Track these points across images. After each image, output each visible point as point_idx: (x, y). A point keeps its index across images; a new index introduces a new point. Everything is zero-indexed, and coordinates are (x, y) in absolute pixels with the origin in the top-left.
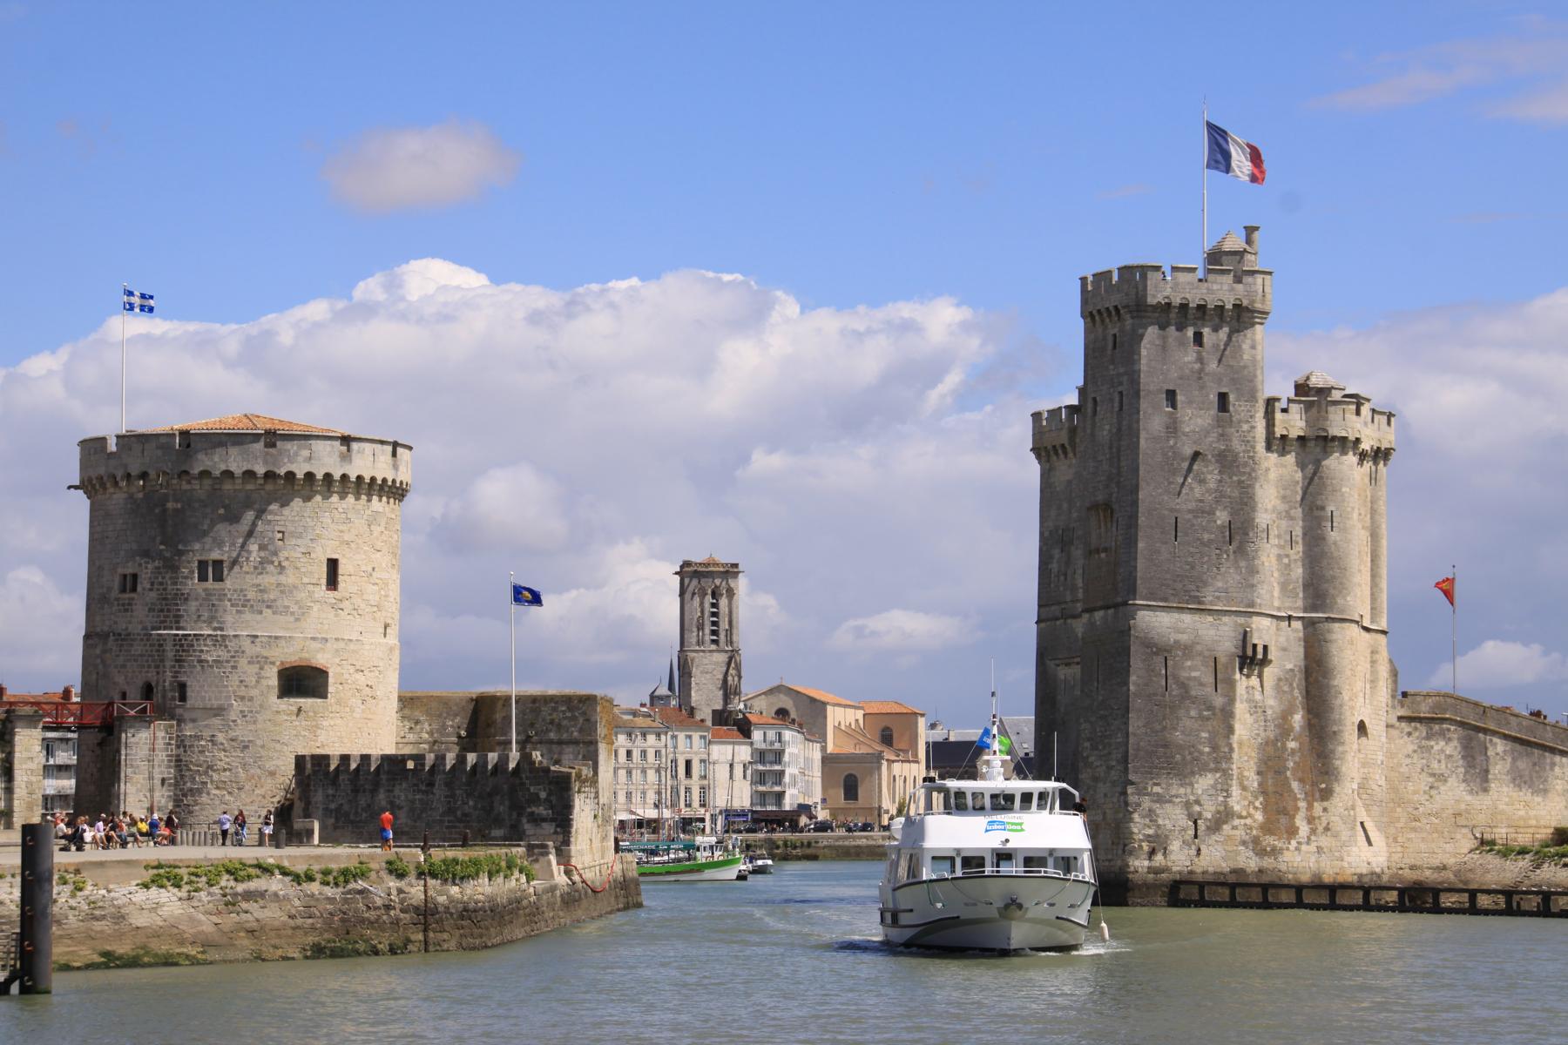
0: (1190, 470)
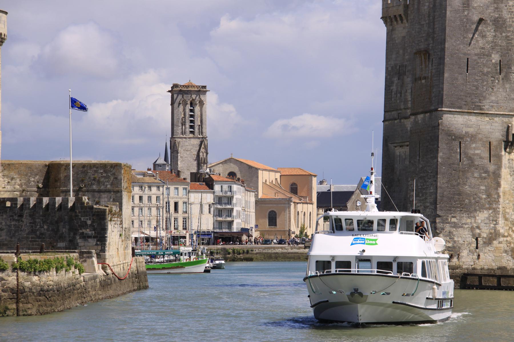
0: (476, 29)
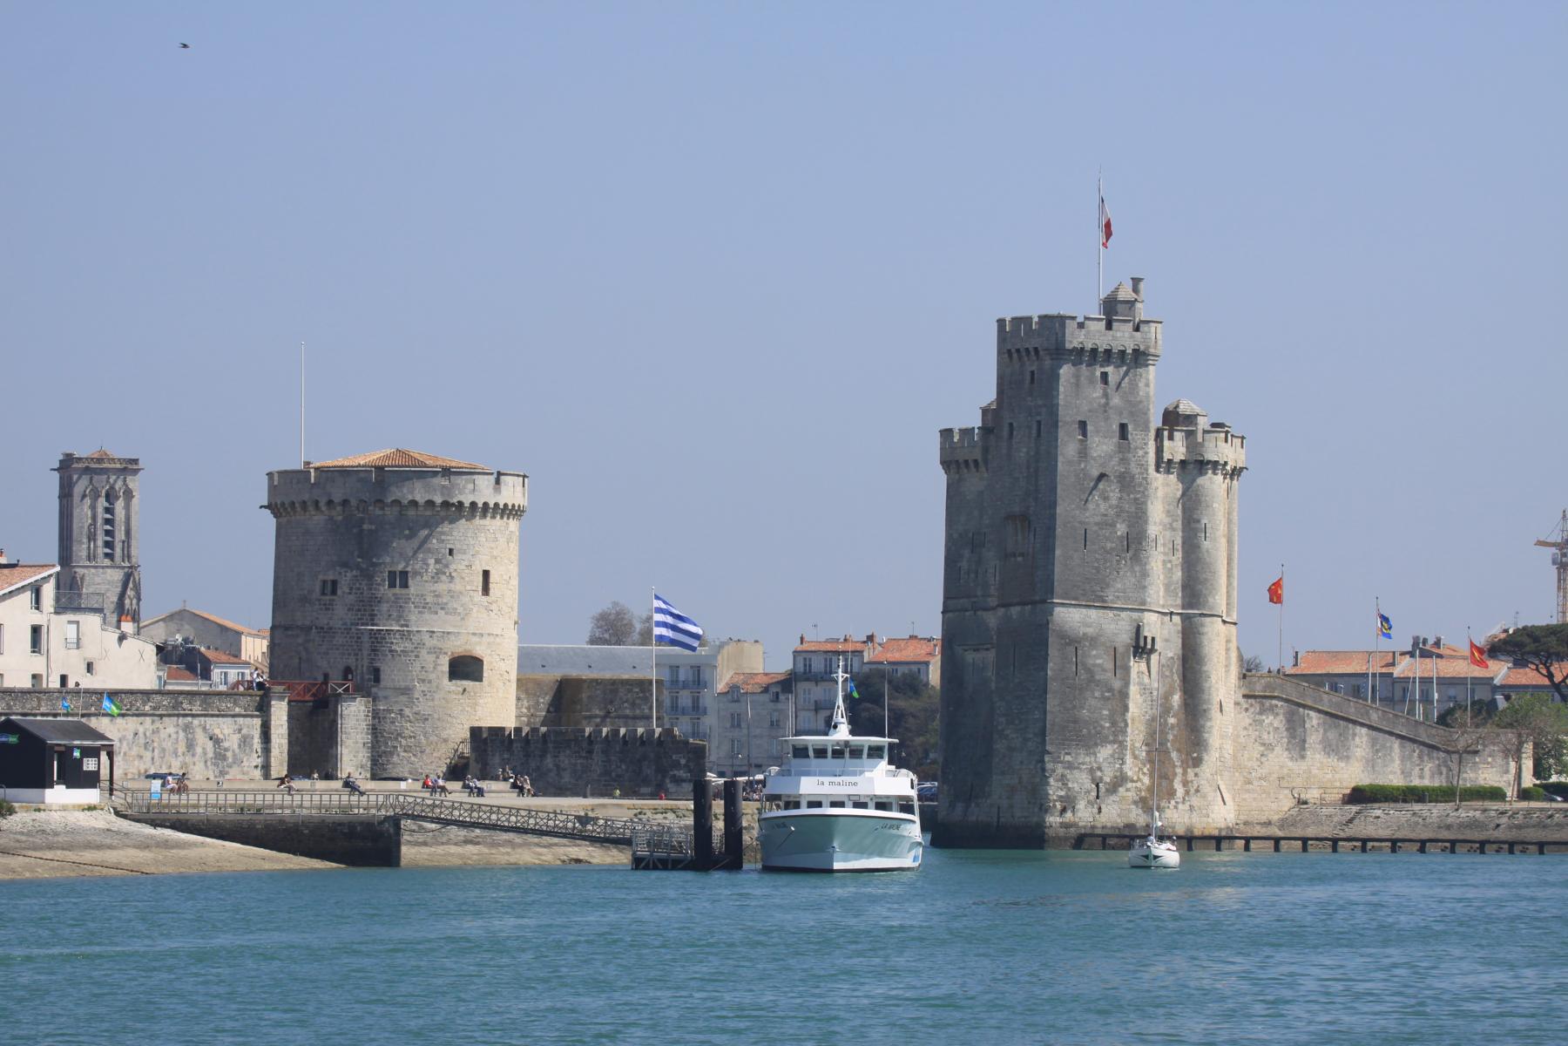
0: (1095, 487)
